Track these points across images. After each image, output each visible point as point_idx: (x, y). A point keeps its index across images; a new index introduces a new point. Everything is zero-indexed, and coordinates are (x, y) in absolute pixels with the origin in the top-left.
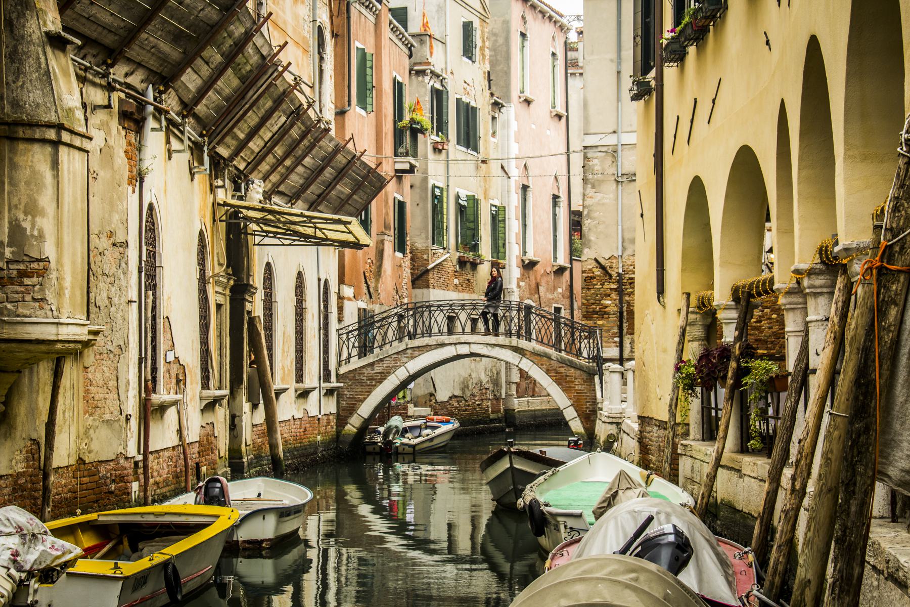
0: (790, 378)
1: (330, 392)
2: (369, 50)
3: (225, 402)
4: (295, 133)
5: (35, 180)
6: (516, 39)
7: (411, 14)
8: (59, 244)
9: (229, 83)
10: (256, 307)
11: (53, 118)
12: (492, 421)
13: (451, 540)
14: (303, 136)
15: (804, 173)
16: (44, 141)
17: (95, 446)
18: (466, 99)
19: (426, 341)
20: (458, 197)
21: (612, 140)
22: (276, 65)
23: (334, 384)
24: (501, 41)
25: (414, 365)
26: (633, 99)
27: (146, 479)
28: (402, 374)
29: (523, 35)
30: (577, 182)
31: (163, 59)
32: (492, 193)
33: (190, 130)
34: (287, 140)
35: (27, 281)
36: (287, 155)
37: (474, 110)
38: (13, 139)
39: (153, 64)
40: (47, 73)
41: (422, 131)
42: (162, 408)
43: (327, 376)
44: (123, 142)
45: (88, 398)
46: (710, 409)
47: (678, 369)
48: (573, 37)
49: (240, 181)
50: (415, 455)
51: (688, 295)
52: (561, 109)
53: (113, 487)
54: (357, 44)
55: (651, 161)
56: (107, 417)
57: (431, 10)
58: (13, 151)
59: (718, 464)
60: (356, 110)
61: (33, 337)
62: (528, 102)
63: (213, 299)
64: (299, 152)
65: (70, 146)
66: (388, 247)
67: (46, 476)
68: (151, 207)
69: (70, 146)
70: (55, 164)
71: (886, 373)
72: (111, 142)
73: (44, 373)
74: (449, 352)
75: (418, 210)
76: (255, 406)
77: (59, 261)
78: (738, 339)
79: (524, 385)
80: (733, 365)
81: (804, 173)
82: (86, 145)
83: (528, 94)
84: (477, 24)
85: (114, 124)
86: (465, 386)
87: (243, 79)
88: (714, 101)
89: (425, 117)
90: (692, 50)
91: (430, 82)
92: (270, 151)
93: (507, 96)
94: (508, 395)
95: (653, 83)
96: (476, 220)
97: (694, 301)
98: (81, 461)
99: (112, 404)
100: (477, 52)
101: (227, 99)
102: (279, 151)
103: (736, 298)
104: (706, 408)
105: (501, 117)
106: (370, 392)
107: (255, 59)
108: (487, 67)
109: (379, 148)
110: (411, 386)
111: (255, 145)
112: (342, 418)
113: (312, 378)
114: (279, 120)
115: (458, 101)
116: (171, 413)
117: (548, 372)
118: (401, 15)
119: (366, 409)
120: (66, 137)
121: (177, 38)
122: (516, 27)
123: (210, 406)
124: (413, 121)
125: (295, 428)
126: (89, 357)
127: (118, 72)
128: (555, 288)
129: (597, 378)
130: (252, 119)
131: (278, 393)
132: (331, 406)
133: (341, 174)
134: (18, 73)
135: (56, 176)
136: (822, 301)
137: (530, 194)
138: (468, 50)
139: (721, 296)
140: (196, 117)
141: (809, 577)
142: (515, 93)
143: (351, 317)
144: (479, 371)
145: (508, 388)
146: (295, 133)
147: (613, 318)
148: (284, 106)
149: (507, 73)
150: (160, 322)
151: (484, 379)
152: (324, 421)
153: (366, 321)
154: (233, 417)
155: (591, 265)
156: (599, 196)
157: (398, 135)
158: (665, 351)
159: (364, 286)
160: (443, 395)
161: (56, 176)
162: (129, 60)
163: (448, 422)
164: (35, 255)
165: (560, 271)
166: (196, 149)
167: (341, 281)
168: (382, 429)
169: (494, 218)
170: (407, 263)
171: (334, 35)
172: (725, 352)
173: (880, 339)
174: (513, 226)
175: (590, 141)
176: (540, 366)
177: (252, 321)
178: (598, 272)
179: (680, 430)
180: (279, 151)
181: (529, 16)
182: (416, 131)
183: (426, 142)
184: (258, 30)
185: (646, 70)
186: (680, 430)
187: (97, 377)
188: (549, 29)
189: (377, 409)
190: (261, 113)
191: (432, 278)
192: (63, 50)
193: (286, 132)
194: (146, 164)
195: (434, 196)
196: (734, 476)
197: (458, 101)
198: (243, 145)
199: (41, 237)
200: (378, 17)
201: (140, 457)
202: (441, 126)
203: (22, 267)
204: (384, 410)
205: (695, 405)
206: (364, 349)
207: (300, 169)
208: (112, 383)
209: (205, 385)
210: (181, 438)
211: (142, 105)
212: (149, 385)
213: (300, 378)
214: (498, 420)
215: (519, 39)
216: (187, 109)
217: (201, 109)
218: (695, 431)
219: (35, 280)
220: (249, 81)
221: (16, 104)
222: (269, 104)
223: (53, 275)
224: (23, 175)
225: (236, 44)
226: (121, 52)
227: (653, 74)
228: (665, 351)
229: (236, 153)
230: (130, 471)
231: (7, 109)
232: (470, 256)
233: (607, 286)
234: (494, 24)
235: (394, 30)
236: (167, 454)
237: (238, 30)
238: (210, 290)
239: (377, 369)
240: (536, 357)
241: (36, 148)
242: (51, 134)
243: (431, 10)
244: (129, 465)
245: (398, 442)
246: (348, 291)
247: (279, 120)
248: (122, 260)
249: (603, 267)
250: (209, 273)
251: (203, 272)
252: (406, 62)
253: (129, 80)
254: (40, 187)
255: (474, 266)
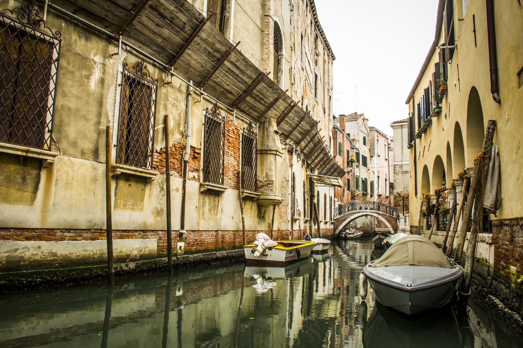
0: (450, 210)
1: (332, 223)
2: (341, 142)
3: (309, 221)
4: (325, 159)
5: (271, 163)
6: (376, 141)
7: (351, 135)
8: (276, 177)
9: (311, 145)
10: (315, 201)
11: (275, 149)
12: (370, 233)
13: (360, 260)
14: (327, 160)
15: (455, 156)
16: (273, 154)
17: (282, 227)
18: (364, 155)
19: (355, 211)
20: (362, 178)
21: (401, 163)
22: (322, 141)
23: (333, 221)
24: (372, 141)
25: (353, 217)
26: (408, 148)
27: (293, 236)
28: (349, 219)
29: (378, 140)
30: (392, 174)
31: (297, 138)
32: (370, 178)
33: (302, 156)
34: (323, 160)
35: (269, 186)
36: (323, 165)
37: (366, 157)
38: (267, 154)
39: (295, 139)
40: (274, 139)
41: (354, 162)
42: (296, 220)
43: (331, 220)
44: (288, 157)
45: (280, 215)
46: (429, 222)
47: (421, 212)
48: (389, 142)
49: (312, 170)
50: (352, 239)
51: (423, 194)
52: (387, 158)
53: (286, 237)
54: (338, 141)
55: (413, 163)
56: (284, 220)
57: (356, 134)
58: (266, 156)
59: (432, 234)
60: (338, 156)
61: (270, 198)
62: (379, 156)
63: (306, 197)
64: (326, 164)
65: (278, 155)
66: (346, 189)
67: (272, 232)
68: (294, 173)
69: (278, 155)
70: (275, 159)
71: (485, 181)
72: (286, 157)
73: (271, 208)
74: (361, 214)
75: (352, 181)
76: (315, 225)
77: (276, 181)
78: (436, 202)
79: (378, 225)
80: (436, 209)
81: (455, 156)
82: (282, 155)
83: (379, 154)
84: (366, 137)
85: (287, 153)
86: (364, 224)
87: (314, 144)
88: (474, 31)
89: (354, 158)
90: (423, 135)
91: (355, 151)
92: (319, 163)
93: (374, 155)
94: (374, 227)
95: (413, 145)
96: (366, 184)
97: (425, 196)
98: (279, 230)
99: (285, 217)
100: (367, 144)
101: (310, 149)
102: (321, 163)
103: (436, 193)
104: (428, 222)
105: (373, 159)
106: (341, 224)
107: (317, 140)
108: (369, 147)
109: (343, 165)
110: (351, 223)
111: (316, 161)
112: (335, 229)
113: (328, 219)
114: (322, 156)
115: (362, 155)
116: (298, 221)
117: (385, 219)
118: (349, 135)
119: (340, 228)
120: (278, 153)
121: (301, 133)
122: (376, 138)
123: (306, 222)
124: (351, 159)
125: (324, 231)
126: (281, 206)
127: (288, 141)
128: (386, 201)
129: (398, 221)
130: (316, 154)
131: (321, 222)
132: (332, 227)
133: (335, 170)
134: (268, 139)
135: (276, 162)
136: (460, 187)
137: (380, 178)
138: (365, 143)
139: (432, 192)
140: (304, 153)
141: (461, 243)
142: (376, 154)
143: (337, 205)
144: (368, 220)
145: (374, 226)
146: (325, 159)
147: (402, 207)
148: (323, 152)
149: (374, 149)
150: (295, 200)
151: (369, 223)
152: (330, 230)
153: (340, 207)
154: (310, 226)
155: (396, 194)
156: (398, 177)
157: (348, 163)
158: (417, 209)
159: (340, 199)
160: (358, 226)
161: (276, 162)
162: (290, 138)
163: (360, 232)
164: (271, 180)
165: (387, 197)
166: (303, 161)
167: (335, 197)
168: (344, 233)
169: (371, 184)
170: (350, 194)
171: (333, 138)
172: (434, 206)
173: (483, 173)
174: (376, 186)
175: (395, 163)
176: (384, 217)
177: (314, 204)
178: (398, 195)
179: (421, 228)
180: (321, 163)
181: (379, 136)
182: (352, 161)
183: (355, 164)
184: (318, 133)
185: (411, 142)
186: (421, 228)
187: (282, 210)
188: (384, 139)
189: (343, 228)
190: (318, 153)
191: (356, 198)
192: (277, 134)
193: (323, 158)
194: (293, 163)
195: (356, 178)
196: (436, 236)
197: (362, 155)
198: (313, 161)
199: (272, 176)
200: (343, 135)
201: (291, 231)
202: (358, 161)
203: (268, 182)
204: (345, 228)
205: (425, 220)
206: (340, 213)
207: (326, 169)
208: (285, 213)
209: (305, 217)
210: (300, 228)
211: (292, 149)
212: (293, 215)
213: (325, 219)
214: (372, 233)
215: (377, 141)
216: (302, 151)
217: (305, 151)
218: (425, 228)
219: (271, 185)
220: (316, 145)
221: (267, 146)
222: (320, 151)
223: (275, 184)
224: (269, 162)
225: (313, 136)
226: (289, 136)
227: (413, 142)
228: (417, 209)
229: (312, 163)
230: (289, 234)
231: (266, 147)
232: (365, 192)
233: (400, 199)
234: (370, 137)
235: (347, 138)
236: (297, 231)
237: (314, 132)
238: (306, 195)
239: (343, 218)
240: (383, 215)
241: (271, 155)
242: (275, 152)
243: (356, 134)
244: (289, 232)
245: (348, 236)
246: (336, 200)
247: (322, 156)
248: (288, 184)
249: (399, 194)
250: (306, 191)
251: (304, 190)
252: (350, 145)
253: (290, 143)
254: (272, 164)
255: (366, 195)
